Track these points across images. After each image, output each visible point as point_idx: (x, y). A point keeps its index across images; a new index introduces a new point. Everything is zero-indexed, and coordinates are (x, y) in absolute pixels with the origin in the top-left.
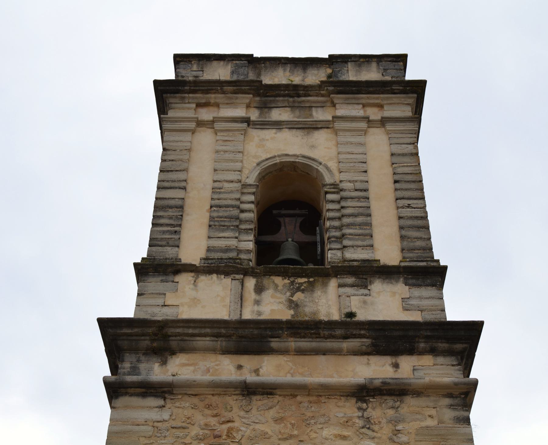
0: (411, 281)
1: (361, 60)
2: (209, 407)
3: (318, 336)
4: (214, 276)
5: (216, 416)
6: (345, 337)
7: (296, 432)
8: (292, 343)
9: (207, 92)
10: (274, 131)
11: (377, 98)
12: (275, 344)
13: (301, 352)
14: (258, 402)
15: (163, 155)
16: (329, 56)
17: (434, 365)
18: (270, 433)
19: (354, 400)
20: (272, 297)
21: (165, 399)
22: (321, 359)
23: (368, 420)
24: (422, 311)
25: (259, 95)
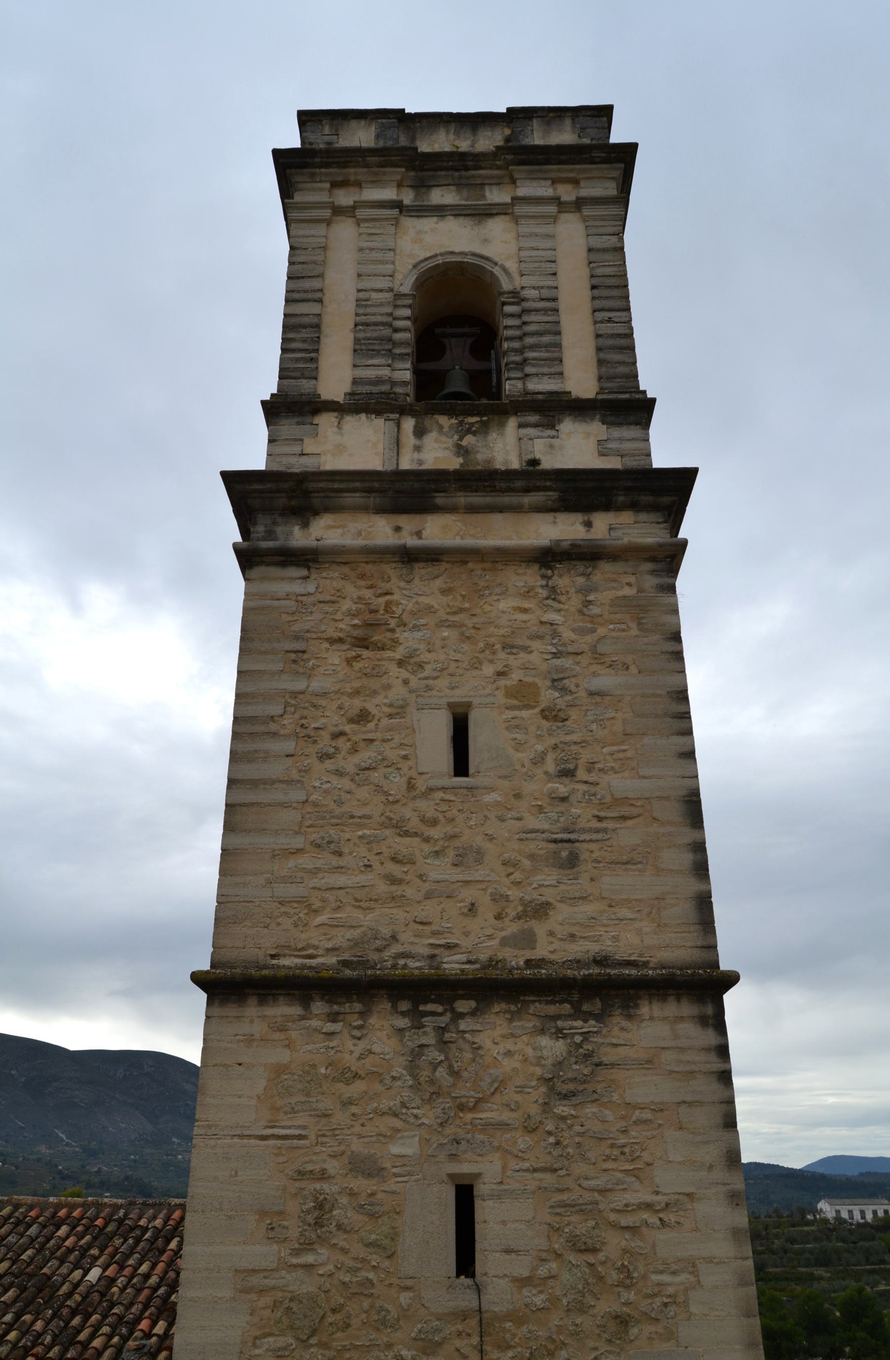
0: (609, 419)
1: (551, 115)
2: (362, 576)
3: (493, 489)
4: (363, 416)
5: (371, 587)
6: (527, 490)
7: (467, 605)
8: (462, 499)
9: (344, 165)
10: (435, 219)
11: (572, 171)
12: (440, 500)
13: (472, 509)
14: (421, 570)
15: (290, 256)
16: (508, 109)
17: (635, 522)
18: (436, 606)
19: (536, 567)
20: (436, 441)
21: (309, 568)
22: (498, 518)
23: (553, 589)
24: (622, 456)
25: (414, 169)
